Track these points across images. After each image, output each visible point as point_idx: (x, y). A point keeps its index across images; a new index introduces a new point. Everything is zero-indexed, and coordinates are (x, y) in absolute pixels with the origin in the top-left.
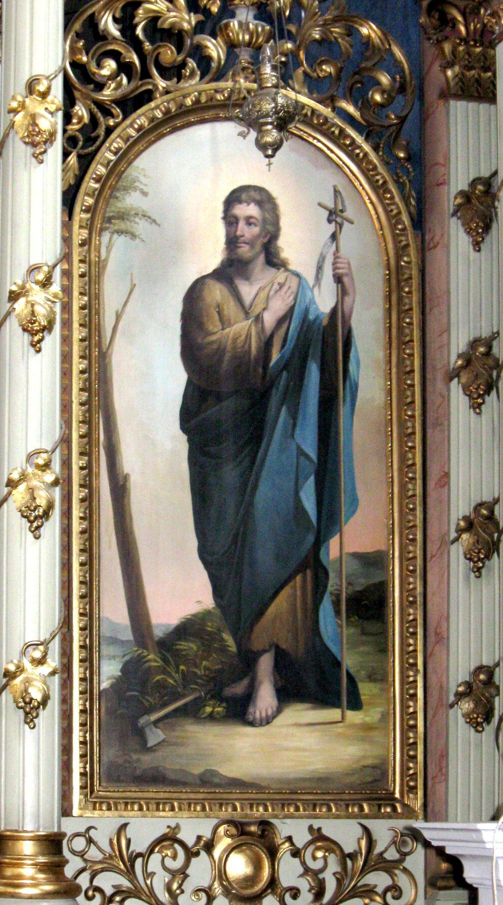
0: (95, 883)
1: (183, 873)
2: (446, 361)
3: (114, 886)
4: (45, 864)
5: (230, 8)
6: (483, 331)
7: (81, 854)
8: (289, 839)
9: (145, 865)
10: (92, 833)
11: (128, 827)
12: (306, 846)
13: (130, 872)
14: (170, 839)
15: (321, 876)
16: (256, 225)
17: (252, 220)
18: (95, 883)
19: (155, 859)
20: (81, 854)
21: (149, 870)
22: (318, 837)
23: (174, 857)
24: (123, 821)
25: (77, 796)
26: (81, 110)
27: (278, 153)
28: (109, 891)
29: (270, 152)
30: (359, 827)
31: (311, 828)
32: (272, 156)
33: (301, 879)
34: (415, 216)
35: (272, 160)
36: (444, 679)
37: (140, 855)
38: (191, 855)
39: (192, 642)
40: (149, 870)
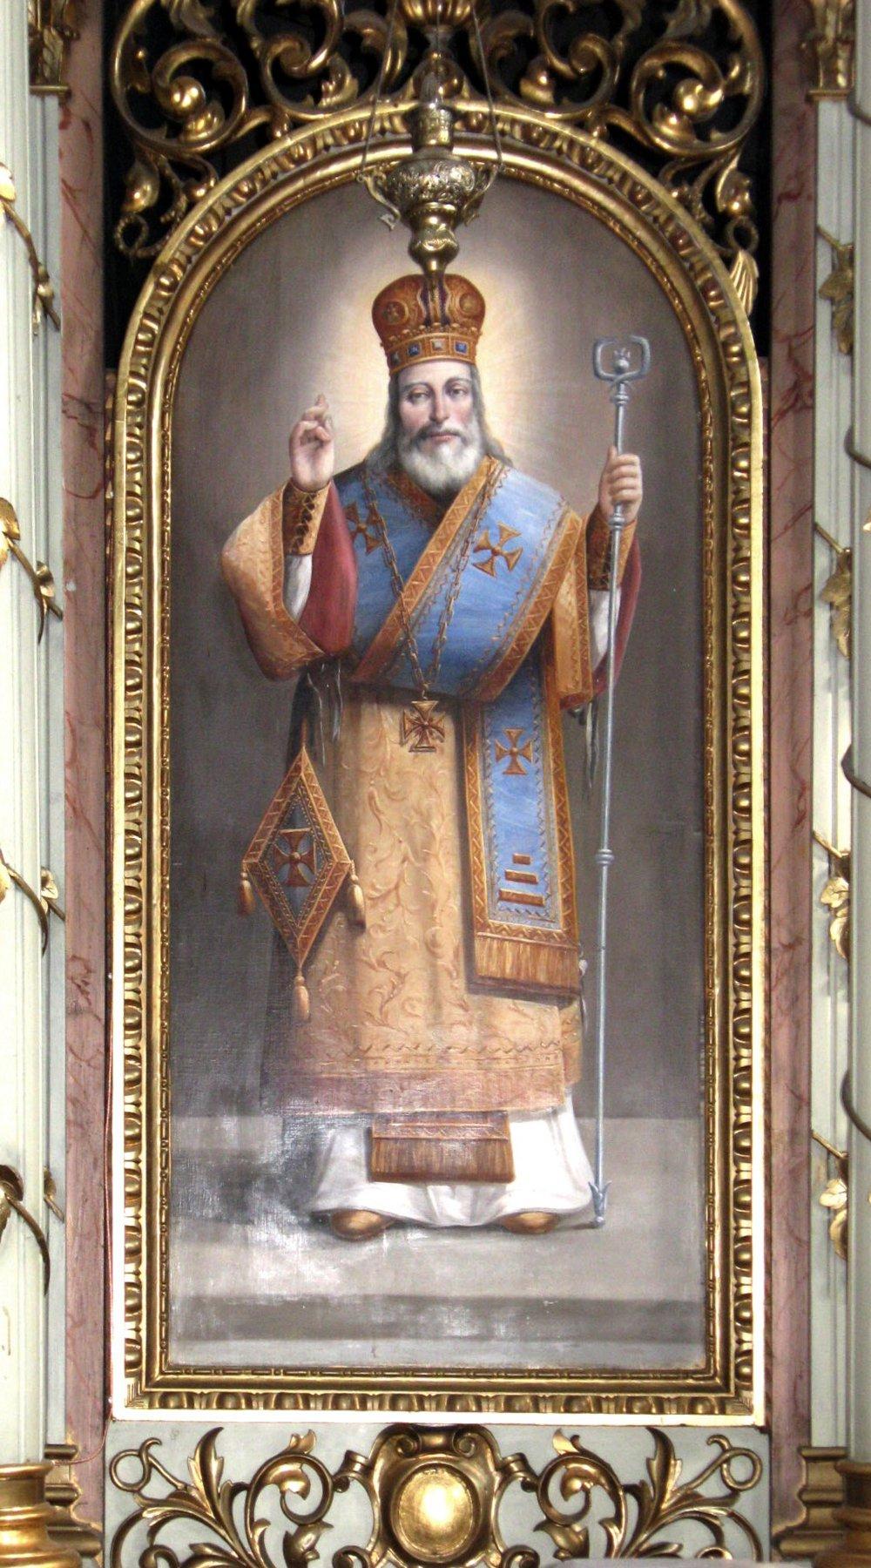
0: (161, 1539)
1: (316, 1521)
2: (804, 1157)
3: (192, 1546)
4: (372, 638)
5: (437, 167)
8: (522, 1459)
9: (250, 1505)
11: (221, 1435)
13: (221, 1522)
18: (161, 1539)
19: (267, 1503)
20: (134, 1489)
21: (258, 1515)
23: (304, 1493)
25: (122, 1385)
26: (109, 406)
28: (183, 1554)
30: (649, 1435)
33: (542, 1535)
37: (237, 1488)
38: (336, 1483)
39: (596, 41)
40: (258, 1515)
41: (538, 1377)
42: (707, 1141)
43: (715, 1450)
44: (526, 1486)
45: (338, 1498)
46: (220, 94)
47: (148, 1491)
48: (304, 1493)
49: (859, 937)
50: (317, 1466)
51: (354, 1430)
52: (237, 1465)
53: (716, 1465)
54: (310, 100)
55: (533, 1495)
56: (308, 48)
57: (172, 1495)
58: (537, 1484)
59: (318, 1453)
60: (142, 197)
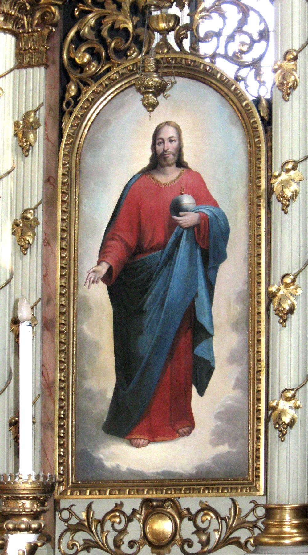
1: (123, 531)
6: (292, 384)
7: (66, 521)
8: (188, 509)
10: (73, 508)
12: (198, 512)
14: (118, 508)
15: (207, 531)
16: (175, 141)
17: (173, 139)
20: (66, 521)
22: (206, 508)
23: (120, 523)
24: (90, 501)
27: (156, 109)
29: (151, 109)
31: (201, 502)
32: (152, 111)
33: (195, 536)
34: (266, 117)
35: (152, 113)
36: (268, 552)
38: (129, 519)
41: (278, 15)
42: (249, 393)
43: (253, 505)
44: (190, 519)
45: (130, 524)
46: (95, 56)
47: (70, 522)
48: (120, 523)
49: (4, 413)
50: (124, 514)
51: (132, 502)
52: (99, 512)
53: (253, 510)
54: (125, 58)
55: (191, 522)
56: (124, 41)
57: (78, 523)
58: (193, 518)
59: (124, 509)
60: (73, 90)
